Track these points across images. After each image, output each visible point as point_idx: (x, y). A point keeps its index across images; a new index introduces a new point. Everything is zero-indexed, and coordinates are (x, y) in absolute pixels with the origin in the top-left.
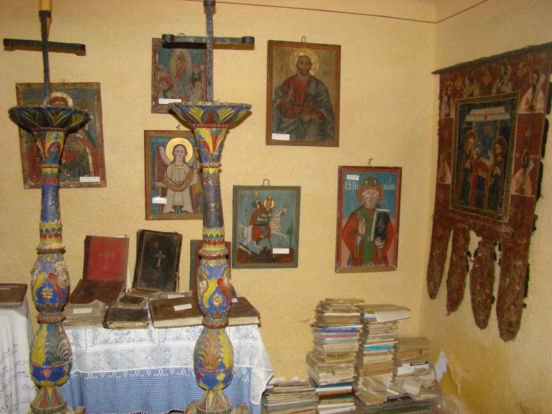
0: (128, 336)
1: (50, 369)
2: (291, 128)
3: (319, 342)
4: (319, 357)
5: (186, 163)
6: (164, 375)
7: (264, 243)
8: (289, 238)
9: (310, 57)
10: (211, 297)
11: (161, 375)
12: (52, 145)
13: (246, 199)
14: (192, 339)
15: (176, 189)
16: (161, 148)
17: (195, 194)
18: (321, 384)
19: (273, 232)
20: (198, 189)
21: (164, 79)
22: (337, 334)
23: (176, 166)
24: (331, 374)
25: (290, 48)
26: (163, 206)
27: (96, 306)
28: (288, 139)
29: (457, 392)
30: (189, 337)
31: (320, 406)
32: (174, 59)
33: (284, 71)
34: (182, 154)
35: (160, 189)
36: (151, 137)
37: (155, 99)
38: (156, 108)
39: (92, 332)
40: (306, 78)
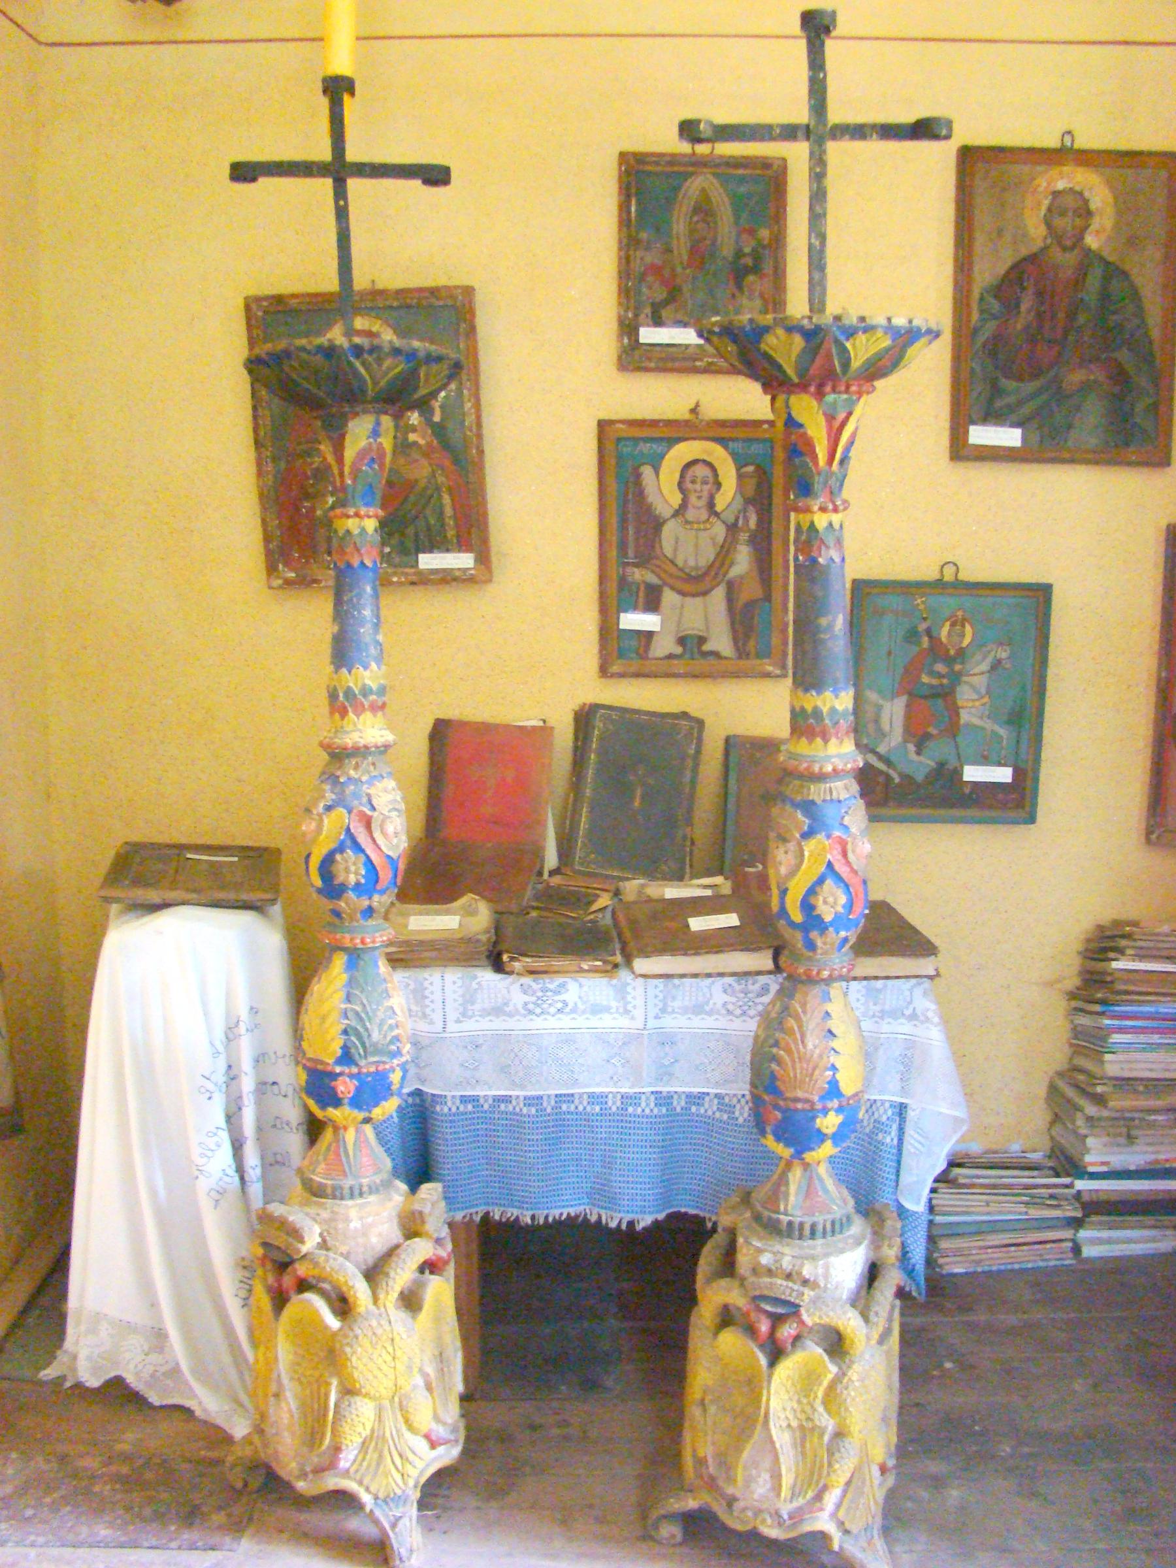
0: (557, 998)
1: (351, 1076)
2: (1027, 409)
3: (1088, 1042)
4: (1090, 1090)
5: (717, 514)
6: (656, 1111)
7: (940, 749)
8: (1014, 734)
9: (1087, 194)
10: (812, 891)
11: (647, 1111)
12: (361, 455)
13: (889, 619)
14: (738, 1012)
15: (687, 587)
16: (647, 471)
17: (741, 603)
18: (1091, 1169)
19: (965, 717)
20: (751, 590)
21: (655, 269)
22: (1154, 1024)
23: (687, 522)
24: (1122, 1140)
25: (1026, 169)
26: (650, 635)
27: (471, 912)
28: (1018, 443)
29: (781, 1315)
30: (730, 1007)
31: (1083, 1234)
32: (684, 209)
33: (1008, 237)
34: (706, 487)
35: (642, 588)
36: (619, 440)
37: (628, 329)
38: (635, 358)
39: (460, 983)
40: (1068, 260)
